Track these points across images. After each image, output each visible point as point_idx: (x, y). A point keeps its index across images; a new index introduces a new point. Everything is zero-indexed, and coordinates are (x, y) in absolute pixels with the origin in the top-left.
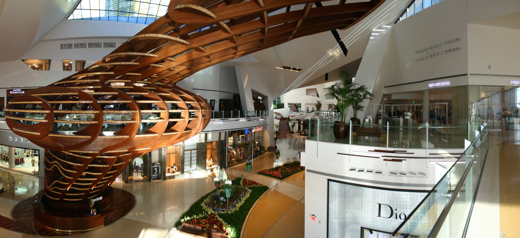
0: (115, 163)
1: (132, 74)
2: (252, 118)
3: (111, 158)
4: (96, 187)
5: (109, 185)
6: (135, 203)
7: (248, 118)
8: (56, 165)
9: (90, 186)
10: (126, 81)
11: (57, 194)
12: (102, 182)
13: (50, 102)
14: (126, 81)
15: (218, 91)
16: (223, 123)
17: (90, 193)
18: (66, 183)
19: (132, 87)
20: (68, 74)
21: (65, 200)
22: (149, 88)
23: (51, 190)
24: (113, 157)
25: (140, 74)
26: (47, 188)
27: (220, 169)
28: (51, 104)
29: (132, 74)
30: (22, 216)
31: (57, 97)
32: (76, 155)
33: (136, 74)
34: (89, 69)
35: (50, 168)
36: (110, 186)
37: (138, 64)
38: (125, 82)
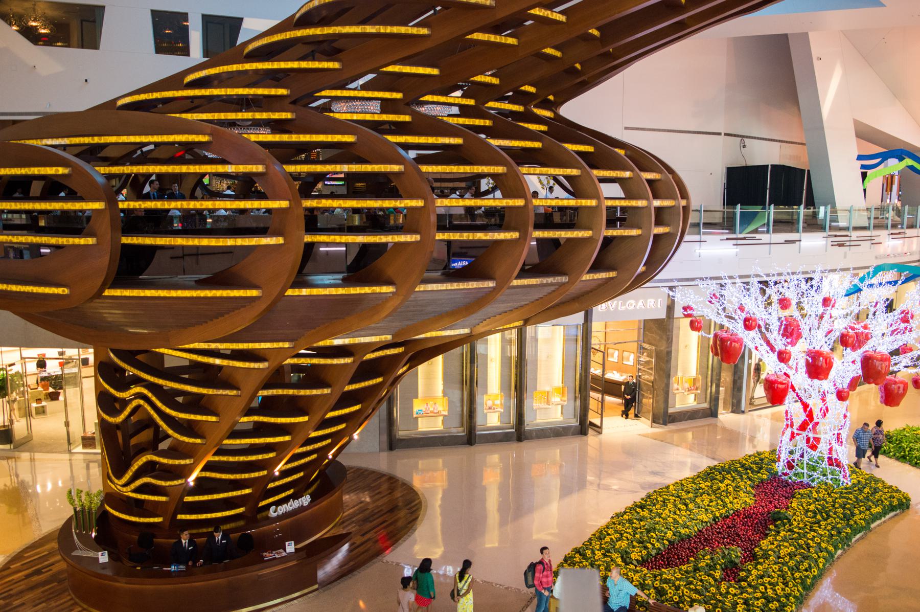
0: (352, 382)
1: (407, 69)
2: (855, 235)
3: (337, 365)
4: (290, 466)
5: (330, 457)
6: (422, 513)
7: (836, 236)
8: (142, 402)
9: (267, 465)
10: (387, 95)
11: (155, 501)
12: (309, 448)
13: (103, 170)
14: (387, 95)
15: (719, 134)
16: (735, 250)
17: (271, 485)
18: (182, 462)
19: (407, 118)
20: (173, 65)
21: (181, 520)
22: (467, 123)
23: (128, 492)
24: (342, 361)
25: (435, 72)
26: (113, 486)
27: (724, 407)
28: (109, 177)
29: (407, 69)
30: (23, 604)
31: (135, 152)
32: (211, 360)
33: (421, 70)
34: (122, 327)
35: (120, 412)
36: (337, 459)
37: (424, 31)
38: (382, 99)
